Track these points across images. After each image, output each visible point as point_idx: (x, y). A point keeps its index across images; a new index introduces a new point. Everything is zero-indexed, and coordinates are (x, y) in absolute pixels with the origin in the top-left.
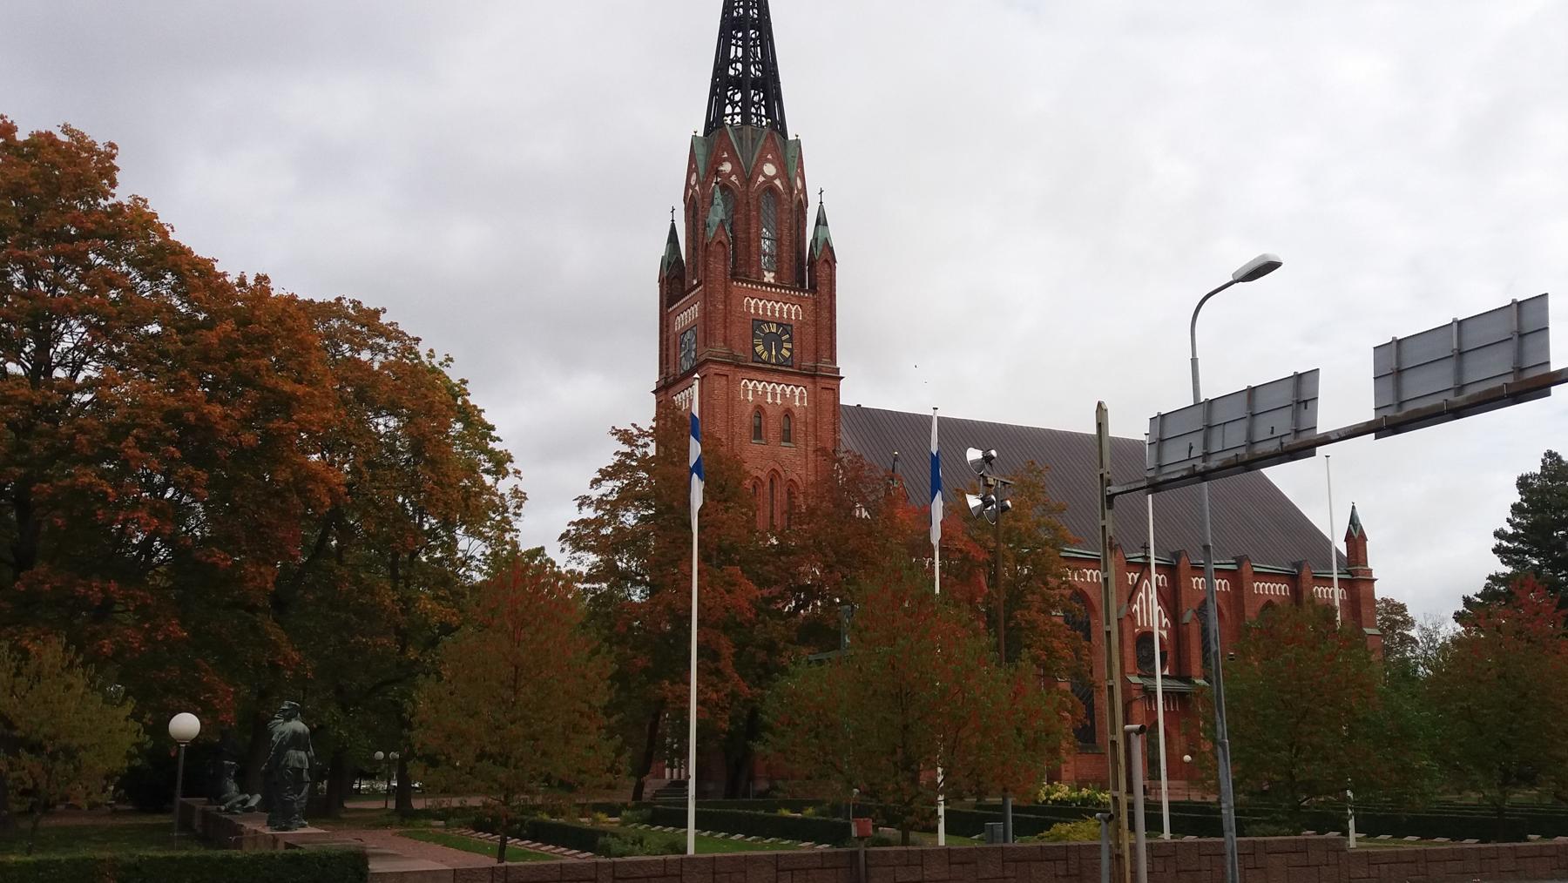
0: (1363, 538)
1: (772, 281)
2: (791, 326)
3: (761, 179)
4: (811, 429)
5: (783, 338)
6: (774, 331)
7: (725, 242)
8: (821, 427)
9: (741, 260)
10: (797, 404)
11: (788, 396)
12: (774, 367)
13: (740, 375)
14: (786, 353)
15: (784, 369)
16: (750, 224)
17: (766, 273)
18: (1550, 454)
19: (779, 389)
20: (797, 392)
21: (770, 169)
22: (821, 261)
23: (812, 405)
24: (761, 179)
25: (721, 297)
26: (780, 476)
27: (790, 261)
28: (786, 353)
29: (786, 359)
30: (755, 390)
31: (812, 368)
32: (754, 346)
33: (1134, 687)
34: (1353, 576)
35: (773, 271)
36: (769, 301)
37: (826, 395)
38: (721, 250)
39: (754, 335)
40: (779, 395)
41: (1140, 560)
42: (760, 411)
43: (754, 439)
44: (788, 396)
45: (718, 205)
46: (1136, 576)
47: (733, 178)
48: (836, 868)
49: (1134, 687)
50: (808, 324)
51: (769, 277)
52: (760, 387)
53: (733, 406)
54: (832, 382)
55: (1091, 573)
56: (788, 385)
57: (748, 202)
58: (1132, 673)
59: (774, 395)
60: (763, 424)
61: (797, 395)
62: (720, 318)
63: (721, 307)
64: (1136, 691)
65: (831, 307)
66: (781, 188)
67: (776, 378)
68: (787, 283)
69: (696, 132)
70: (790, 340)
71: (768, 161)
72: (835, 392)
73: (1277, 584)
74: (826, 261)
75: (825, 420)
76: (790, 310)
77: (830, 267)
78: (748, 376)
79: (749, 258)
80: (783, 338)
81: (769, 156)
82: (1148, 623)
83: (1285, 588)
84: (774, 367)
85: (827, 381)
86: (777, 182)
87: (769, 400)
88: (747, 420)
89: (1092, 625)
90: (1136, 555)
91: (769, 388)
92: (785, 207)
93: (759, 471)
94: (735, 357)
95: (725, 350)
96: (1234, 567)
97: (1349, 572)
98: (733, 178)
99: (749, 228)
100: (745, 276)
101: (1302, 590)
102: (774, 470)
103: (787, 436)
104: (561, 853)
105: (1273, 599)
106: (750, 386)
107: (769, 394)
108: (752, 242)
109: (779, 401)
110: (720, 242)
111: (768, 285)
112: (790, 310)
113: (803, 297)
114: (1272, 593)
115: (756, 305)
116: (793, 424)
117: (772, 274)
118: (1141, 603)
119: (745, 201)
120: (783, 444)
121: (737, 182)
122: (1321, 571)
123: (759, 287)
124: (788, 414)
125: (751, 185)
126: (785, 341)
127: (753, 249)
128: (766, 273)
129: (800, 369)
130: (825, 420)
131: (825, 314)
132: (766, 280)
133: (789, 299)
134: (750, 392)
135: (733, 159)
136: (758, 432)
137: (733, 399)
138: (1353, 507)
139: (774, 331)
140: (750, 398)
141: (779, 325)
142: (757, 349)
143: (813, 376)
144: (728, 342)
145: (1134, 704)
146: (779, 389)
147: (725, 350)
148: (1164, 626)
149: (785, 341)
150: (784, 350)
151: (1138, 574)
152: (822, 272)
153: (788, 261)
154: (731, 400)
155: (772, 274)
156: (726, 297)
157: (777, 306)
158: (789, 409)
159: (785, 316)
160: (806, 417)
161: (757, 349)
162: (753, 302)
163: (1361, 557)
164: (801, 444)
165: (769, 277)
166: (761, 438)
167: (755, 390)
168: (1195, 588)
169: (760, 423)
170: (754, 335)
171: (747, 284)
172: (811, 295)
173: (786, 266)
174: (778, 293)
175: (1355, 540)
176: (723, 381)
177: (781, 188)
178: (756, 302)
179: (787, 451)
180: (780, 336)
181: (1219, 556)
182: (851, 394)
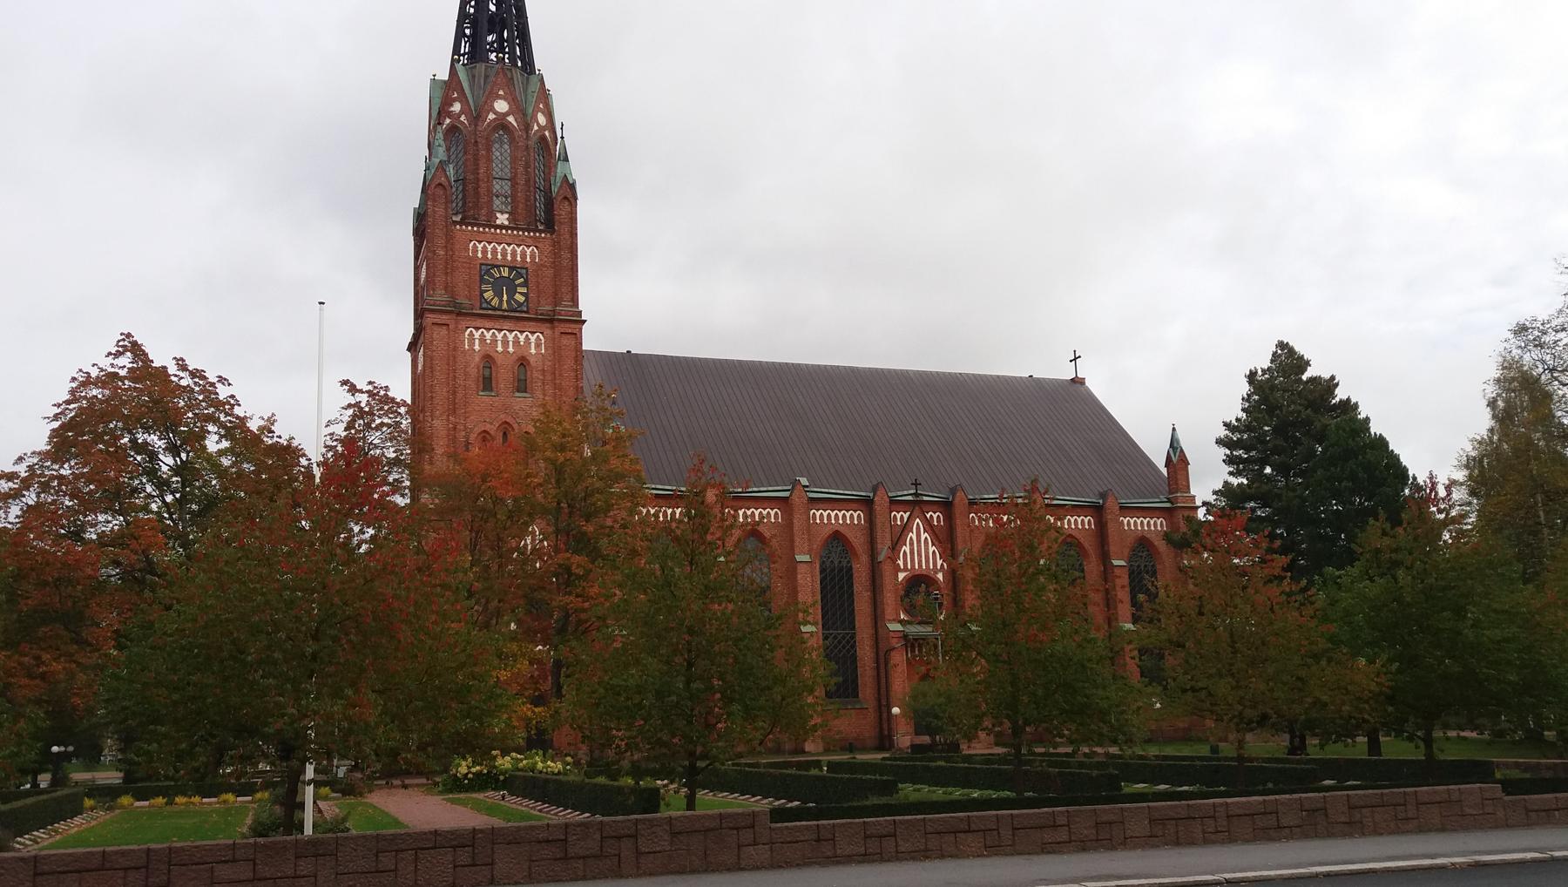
0: (1184, 461)
1: (506, 223)
2: (526, 268)
3: (491, 116)
4: (549, 377)
5: (517, 282)
6: (506, 275)
7: (446, 184)
8: (560, 375)
9: (469, 202)
10: (533, 351)
11: (522, 343)
12: (506, 314)
13: (463, 324)
14: (521, 299)
15: (517, 315)
16: (478, 165)
17: (498, 215)
18: (1282, 345)
19: (511, 337)
20: (533, 338)
21: (501, 106)
22: (559, 199)
23: (550, 351)
24: (491, 116)
25: (441, 242)
26: (513, 429)
27: (526, 200)
28: (521, 299)
29: (520, 304)
30: (482, 339)
31: (550, 313)
32: (482, 292)
33: (891, 634)
34: (1172, 503)
35: (507, 212)
36: (500, 244)
37: (566, 341)
38: (442, 193)
39: (482, 281)
40: (511, 343)
41: (910, 498)
42: (488, 360)
43: (482, 391)
44: (522, 343)
45: (439, 146)
46: (906, 516)
47: (463, 118)
48: (737, 829)
49: (891, 634)
50: (546, 266)
51: (502, 219)
52: (488, 335)
53: (454, 358)
54: (573, 326)
55: (1083, 520)
56: (522, 332)
57: (476, 142)
58: (894, 620)
59: (505, 342)
60: (494, 375)
61: (533, 342)
62: (441, 264)
63: (442, 253)
64: (895, 640)
65: (572, 247)
66: (516, 125)
67: (507, 325)
68: (522, 224)
69: (434, 76)
70: (525, 284)
71: (500, 97)
72: (577, 337)
73: (772, 509)
74: (566, 198)
75: (565, 367)
76: (525, 252)
77: (571, 204)
78: (474, 324)
79: (478, 199)
80: (517, 282)
81: (501, 92)
82: (920, 565)
83: (1089, 521)
84: (506, 314)
85: (567, 325)
86: (511, 119)
87: (500, 349)
88: (473, 371)
89: (854, 571)
90: (906, 493)
91: (500, 336)
92: (520, 144)
93: (488, 425)
94: (455, 305)
95: (446, 298)
96: (786, 494)
97: (1169, 501)
98: (463, 118)
99: (478, 169)
100: (475, 219)
101: (1106, 523)
102: (506, 422)
103: (522, 386)
104: (735, 798)
105: (842, 530)
106: (477, 335)
107: (499, 343)
108: (481, 183)
109: (511, 349)
110: (440, 184)
111: (502, 227)
112: (525, 252)
113: (540, 237)
114: (1073, 526)
115: (482, 249)
116: (529, 373)
117: (506, 216)
118: (912, 544)
119: (473, 141)
120: (517, 394)
121: (466, 122)
122: (1129, 501)
123: (487, 230)
124: (523, 362)
125: (480, 124)
126: (519, 285)
127: (482, 191)
128: (498, 215)
129: (536, 314)
130: (565, 367)
131: (566, 255)
132: (498, 222)
133: (523, 240)
134: (477, 341)
135: (463, 98)
136: (487, 383)
137: (455, 349)
138: (1174, 429)
139: (506, 275)
140: (477, 347)
141: (512, 269)
142: (486, 295)
143: (551, 321)
144: (449, 289)
145: (893, 653)
146: (511, 337)
147: (446, 298)
148: (939, 567)
149: (519, 285)
150: (517, 294)
151: (908, 513)
152: (561, 211)
153: (523, 201)
154: (454, 349)
155: (506, 216)
156: (447, 242)
157: (509, 249)
158: (523, 357)
159: (519, 259)
160: (544, 365)
161: (486, 295)
162: (480, 247)
163: (1182, 482)
164: (539, 394)
165: (502, 219)
166: (491, 390)
167: (482, 339)
168: (1126, 528)
169: (491, 374)
170: (482, 281)
171: (472, 227)
172: (549, 235)
173: (521, 206)
174: (510, 235)
175: (1174, 465)
176: (444, 331)
177: (516, 125)
178: (484, 245)
179: (521, 402)
180: (514, 280)
181: (1064, 492)
182: (593, 339)
